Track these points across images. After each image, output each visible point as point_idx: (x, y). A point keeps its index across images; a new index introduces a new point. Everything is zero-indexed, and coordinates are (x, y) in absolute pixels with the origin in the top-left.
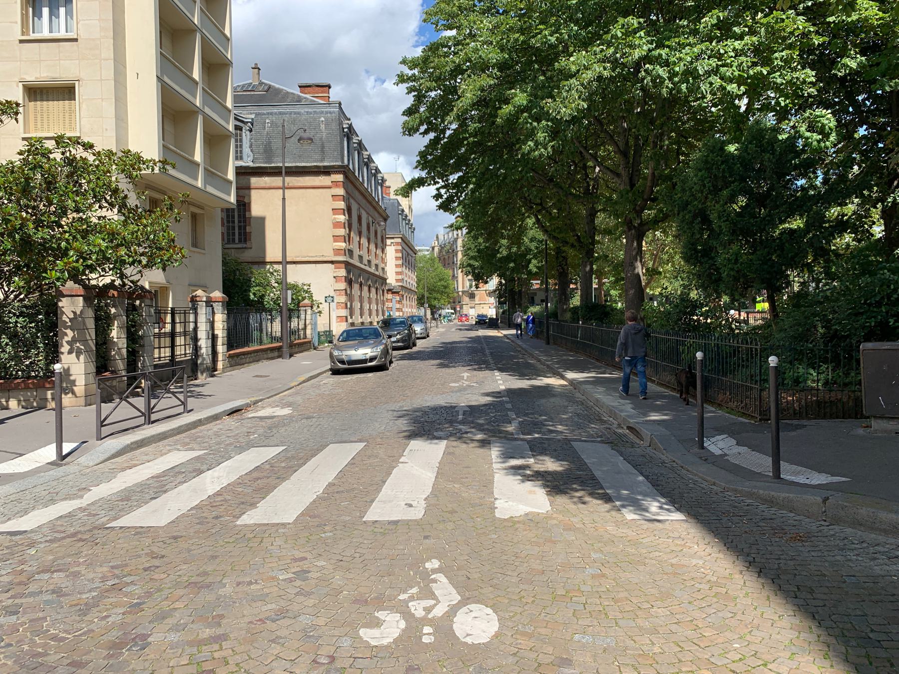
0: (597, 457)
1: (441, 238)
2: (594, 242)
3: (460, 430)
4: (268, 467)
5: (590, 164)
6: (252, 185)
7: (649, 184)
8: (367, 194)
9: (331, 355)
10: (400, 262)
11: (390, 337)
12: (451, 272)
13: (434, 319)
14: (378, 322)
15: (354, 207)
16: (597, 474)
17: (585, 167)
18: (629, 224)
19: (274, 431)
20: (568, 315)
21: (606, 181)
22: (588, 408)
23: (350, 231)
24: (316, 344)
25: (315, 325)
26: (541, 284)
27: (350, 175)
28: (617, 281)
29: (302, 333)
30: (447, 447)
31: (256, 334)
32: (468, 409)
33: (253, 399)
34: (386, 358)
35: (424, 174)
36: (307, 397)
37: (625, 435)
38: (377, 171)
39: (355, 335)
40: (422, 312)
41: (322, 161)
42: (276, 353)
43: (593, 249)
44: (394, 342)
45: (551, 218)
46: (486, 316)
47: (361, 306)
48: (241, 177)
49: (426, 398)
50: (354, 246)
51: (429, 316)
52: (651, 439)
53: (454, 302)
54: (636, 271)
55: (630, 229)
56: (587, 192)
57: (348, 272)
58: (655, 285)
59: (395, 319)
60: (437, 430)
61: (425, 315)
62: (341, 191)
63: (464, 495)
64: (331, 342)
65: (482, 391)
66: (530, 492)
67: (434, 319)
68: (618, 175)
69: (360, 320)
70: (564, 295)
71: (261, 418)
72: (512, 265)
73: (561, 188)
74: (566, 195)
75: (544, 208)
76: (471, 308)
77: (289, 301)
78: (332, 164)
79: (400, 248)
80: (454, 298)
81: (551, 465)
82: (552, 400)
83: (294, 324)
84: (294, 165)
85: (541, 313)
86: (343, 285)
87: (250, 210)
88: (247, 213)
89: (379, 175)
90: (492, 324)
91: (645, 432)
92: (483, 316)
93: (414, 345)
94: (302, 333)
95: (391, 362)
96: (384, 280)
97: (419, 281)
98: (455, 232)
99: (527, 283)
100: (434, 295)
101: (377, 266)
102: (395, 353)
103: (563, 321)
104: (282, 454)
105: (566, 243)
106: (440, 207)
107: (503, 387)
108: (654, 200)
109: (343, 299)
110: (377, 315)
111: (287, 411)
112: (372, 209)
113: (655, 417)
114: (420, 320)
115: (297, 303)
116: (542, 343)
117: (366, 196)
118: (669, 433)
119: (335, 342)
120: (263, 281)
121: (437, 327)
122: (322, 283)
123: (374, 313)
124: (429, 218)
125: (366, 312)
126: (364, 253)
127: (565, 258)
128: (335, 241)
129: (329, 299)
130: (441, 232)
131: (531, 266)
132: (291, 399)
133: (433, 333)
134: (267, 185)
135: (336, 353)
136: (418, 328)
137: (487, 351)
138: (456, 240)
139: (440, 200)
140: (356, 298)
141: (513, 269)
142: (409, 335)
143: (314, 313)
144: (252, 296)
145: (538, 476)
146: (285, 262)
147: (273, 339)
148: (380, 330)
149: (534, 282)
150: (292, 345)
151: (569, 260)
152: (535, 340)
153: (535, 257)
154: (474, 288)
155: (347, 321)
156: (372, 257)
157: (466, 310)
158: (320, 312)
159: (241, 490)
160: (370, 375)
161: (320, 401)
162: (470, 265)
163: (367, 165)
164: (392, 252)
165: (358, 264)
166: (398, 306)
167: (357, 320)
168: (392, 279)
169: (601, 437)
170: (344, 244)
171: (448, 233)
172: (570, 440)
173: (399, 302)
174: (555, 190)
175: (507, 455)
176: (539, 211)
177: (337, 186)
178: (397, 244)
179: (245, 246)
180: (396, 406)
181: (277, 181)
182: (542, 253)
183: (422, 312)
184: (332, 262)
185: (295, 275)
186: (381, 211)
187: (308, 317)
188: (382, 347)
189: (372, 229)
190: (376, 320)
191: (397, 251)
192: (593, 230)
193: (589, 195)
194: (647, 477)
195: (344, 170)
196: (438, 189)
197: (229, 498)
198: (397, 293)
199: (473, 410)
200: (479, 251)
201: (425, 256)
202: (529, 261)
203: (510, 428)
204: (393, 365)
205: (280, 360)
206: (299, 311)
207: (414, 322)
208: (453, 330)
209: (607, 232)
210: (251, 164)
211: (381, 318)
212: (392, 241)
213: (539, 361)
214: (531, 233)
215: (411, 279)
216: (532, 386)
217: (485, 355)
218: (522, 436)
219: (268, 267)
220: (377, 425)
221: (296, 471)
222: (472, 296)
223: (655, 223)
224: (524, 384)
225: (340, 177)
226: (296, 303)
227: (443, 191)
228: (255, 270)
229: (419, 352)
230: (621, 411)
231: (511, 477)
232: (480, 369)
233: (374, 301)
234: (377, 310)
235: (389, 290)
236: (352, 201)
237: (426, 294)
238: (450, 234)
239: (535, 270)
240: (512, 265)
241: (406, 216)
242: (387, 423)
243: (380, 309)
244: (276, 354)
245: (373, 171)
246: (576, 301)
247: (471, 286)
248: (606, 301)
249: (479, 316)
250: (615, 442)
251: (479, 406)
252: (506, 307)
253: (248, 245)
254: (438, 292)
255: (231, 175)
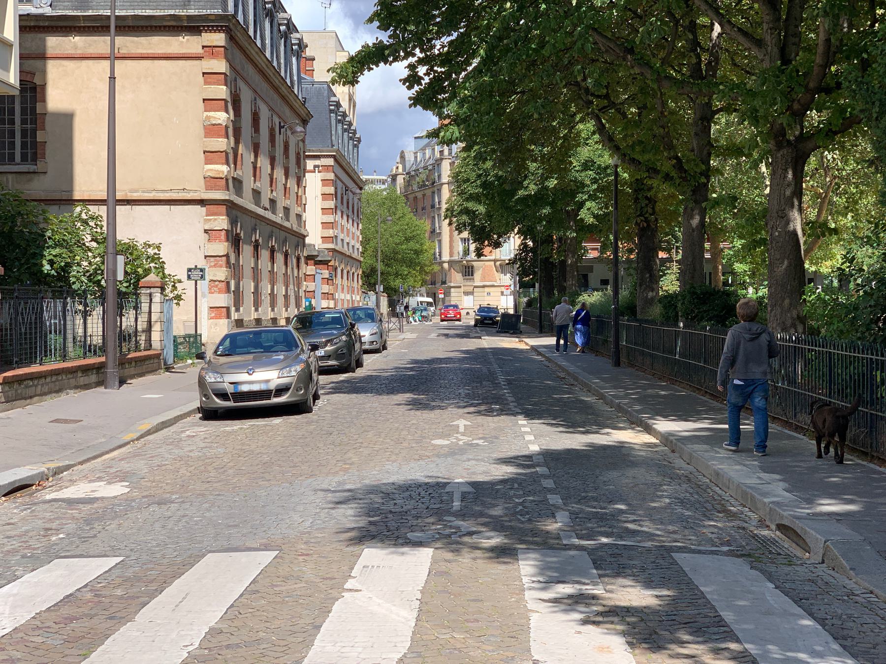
0: (723, 582)
1: (410, 158)
2: (708, 172)
3: (458, 528)
4: (89, 596)
5: (703, 20)
6: (50, 52)
7: (819, 60)
8: (270, 73)
9: (202, 382)
10: (331, 204)
11: (315, 348)
12: (428, 227)
13: (393, 313)
14: (288, 320)
15: (246, 96)
16: (728, 616)
17: (693, 27)
18: (778, 136)
19: (97, 526)
20: (656, 311)
21: (732, 55)
22: (700, 488)
23: (237, 142)
24: (170, 361)
25: (167, 323)
26: (603, 250)
27: (239, 36)
28: (749, 248)
29: (142, 338)
30: (434, 561)
31: (54, 339)
32: (470, 489)
33: (53, 465)
34: (307, 388)
35: (384, 37)
36: (157, 461)
37: (774, 542)
38: (291, 27)
39: (246, 343)
40: (371, 301)
41: (185, 6)
42: (94, 376)
43: (705, 185)
44: (322, 358)
45: (629, 124)
46: (495, 310)
47: (256, 287)
48: (29, 36)
49: (388, 466)
50: (245, 172)
51: (384, 308)
52: (826, 549)
53: (433, 283)
54: (791, 227)
55: (779, 146)
56: (696, 71)
57: (233, 222)
58: (820, 254)
59: (321, 314)
60: (412, 529)
61: (378, 305)
62: (220, 66)
63: (476, 653)
64: (201, 356)
65: (496, 455)
66: (601, 649)
67: (393, 313)
68: (759, 43)
69: (254, 315)
70: (648, 271)
71: (70, 502)
72: (546, 211)
73: (648, 65)
74: (659, 80)
75: (612, 105)
76: (466, 293)
77: (120, 276)
78: (204, 12)
79: (331, 176)
80: (434, 275)
81: (633, 595)
82: (631, 472)
83: (127, 321)
84: (130, 13)
85: (602, 306)
86: (221, 247)
87: (44, 100)
88: (39, 105)
89: (295, 35)
90: (507, 325)
91: (815, 536)
92: (489, 309)
93: (359, 364)
94: (142, 338)
95: (316, 397)
96: (300, 238)
97: (365, 242)
98: (437, 149)
99: (575, 247)
100: (394, 270)
101: (287, 210)
102: (323, 379)
103: (647, 321)
104: (117, 572)
105: (653, 171)
106: (416, 101)
107: (535, 448)
108: (828, 91)
109: (221, 273)
110: (287, 306)
111: (118, 489)
112: (280, 101)
113: (829, 506)
114: (370, 316)
115: (135, 280)
116: (604, 363)
117: (269, 77)
118: (858, 538)
119: (209, 354)
120: (68, 237)
121: (401, 329)
122: (182, 241)
123: (280, 301)
124: (390, 116)
125: (266, 300)
126: (263, 185)
127: (652, 201)
128: (208, 162)
129: (195, 273)
130: (410, 147)
131: (583, 214)
132: (125, 466)
133: (394, 341)
134: (79, 52)
135: (210, 378)
136: (366, 332)
137: (501, 378)
138: (438, 162)
139: (416, 88)
140: (247, 272)
141: (550, 219)
142: (350, 345)
143: (166, 301)
144: (47, 267)
145: (614, 614)
146: (113, 201)
147: (88, 349)
148: (296, 334)
149: (589, 245)
150: (125, 360)
151: (659, 206)
152: (591, 357)
153: (592, 197)
154: (473, 256)
155: (228, 316)
156: (278, 194)
157: (455, 297)
158: (178, 298)
159: (39, 640)
160: (277, 421)
161: (183, 471)
162: (466, 211)
163: (271, 15)
164: (315, 184)
165: (252, 207)
166: (326, 288)
167: (249, 314)
168: (315, 237)
169: (728, 543)
170: (224, 169)
171: (423, 149)
172: (670, 550)
173: (329, 280)
174: (637, 70)
175: (552, 576)
176: (603, 109)
177: (213, 55)
178: (327, 168)
179: (32, 168)
180: (331, 482)
181: (99, 44)
182: (611, 191)
183: (371, 301)
184: (202, 202)
185: (132, 227)
186: (297, 105)
187: (156, 308)
188: (299, 368)
189: (279, 140)
190: (285, 315)
191: (324, 182)
192: (708, 147)
193: (701, 78)
194: (822, 622)
195: (226, 24)
196: (412, 67)
197: (19, 655)
198: (325, 263)
199: (480, 493)
200: (484, 185)
201: (377, 193)
202: (581, 205)
203: (553, 526)
204: (319, 403)
205: (101, 389)
206: (137, 295)
207: (359, 319)
208: (433, 335)
209: (735, 150)
210: (48, 11)
211: (293, 312)
212: (317, 162)
213: (602, 397)
214: (585, 153)
215: (351, 237)
216: (591, 445)
217: (497, 385)
218: (576, 541)
219: (78, 209)
220: (296, 518)
221: (145, 604)
222: (468, 271)
223: (829, 135)
224: (576, 441)
225: (218, 39)
226: (133, 279)
227: (422, 70)
228: (54, 215)
229: (368, 379)
230: (766, 494)
231: (564, 617)
232: (489, 412)
233: (280, 278)
234: (286, 296)
235: (309, 258)
236: (241, 84)
237: (380, 267)
238: (428, 152)
239: (591, 220)
240: (546, 211)
241: (344, 115)
242: (314, 510)
243: (291, 293)
244: (93, 378)
245: (283, 28)
246: (670, 283)
247: (466, 252)
248: (725, 283)
249: (481, 309)
250: (756, 554)
251: (492, 484)
252: (534, 293)
253: (40, 166)
254: (403, 261)
255: (10, 32)
